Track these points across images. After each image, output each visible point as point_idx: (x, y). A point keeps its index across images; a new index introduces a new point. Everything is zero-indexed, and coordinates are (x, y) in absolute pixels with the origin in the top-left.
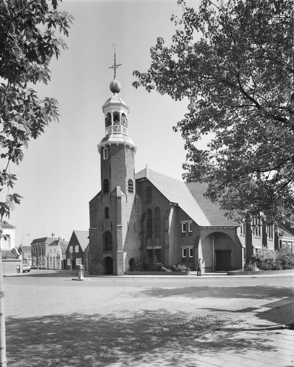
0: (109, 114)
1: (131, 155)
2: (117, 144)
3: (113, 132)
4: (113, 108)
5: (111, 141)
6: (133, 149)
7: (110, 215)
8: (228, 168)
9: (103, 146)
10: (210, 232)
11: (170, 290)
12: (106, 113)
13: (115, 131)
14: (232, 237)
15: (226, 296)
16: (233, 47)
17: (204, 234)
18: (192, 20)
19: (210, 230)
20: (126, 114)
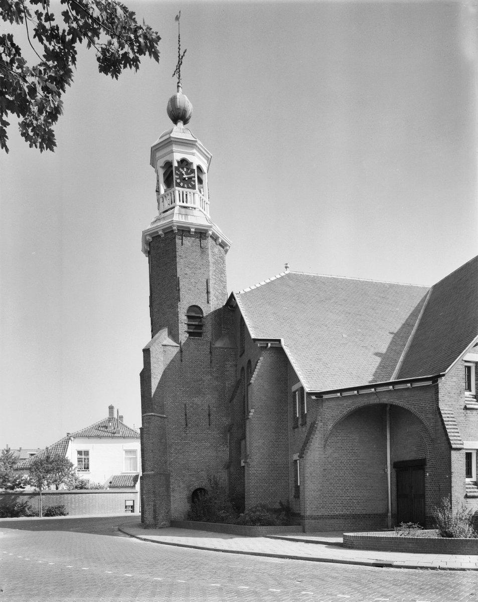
0: (168, 165)
1: (198, 250)
2: (193, 230)
3: (178, 203)
4: (179, 152)
5: (177, 222)
6: (223, 245)
7: (108, 410)
8: (165, 234)
9: (157, 232)
10: (349, 406)
11: (15, 517)
12: (161, 163)
13: (183, 202)
14: (422, 417)
15: (278, 522)
16: (122, 64)
17: (329, 415)
18: (157, 33)
19: (350, 401)
20: (205, 168)
